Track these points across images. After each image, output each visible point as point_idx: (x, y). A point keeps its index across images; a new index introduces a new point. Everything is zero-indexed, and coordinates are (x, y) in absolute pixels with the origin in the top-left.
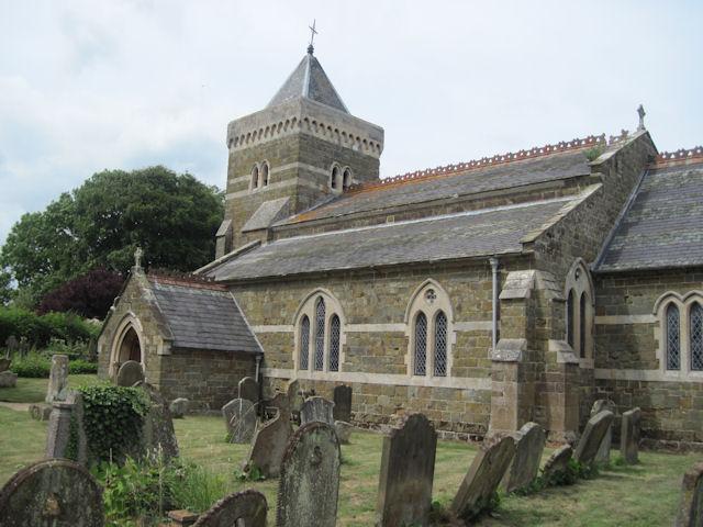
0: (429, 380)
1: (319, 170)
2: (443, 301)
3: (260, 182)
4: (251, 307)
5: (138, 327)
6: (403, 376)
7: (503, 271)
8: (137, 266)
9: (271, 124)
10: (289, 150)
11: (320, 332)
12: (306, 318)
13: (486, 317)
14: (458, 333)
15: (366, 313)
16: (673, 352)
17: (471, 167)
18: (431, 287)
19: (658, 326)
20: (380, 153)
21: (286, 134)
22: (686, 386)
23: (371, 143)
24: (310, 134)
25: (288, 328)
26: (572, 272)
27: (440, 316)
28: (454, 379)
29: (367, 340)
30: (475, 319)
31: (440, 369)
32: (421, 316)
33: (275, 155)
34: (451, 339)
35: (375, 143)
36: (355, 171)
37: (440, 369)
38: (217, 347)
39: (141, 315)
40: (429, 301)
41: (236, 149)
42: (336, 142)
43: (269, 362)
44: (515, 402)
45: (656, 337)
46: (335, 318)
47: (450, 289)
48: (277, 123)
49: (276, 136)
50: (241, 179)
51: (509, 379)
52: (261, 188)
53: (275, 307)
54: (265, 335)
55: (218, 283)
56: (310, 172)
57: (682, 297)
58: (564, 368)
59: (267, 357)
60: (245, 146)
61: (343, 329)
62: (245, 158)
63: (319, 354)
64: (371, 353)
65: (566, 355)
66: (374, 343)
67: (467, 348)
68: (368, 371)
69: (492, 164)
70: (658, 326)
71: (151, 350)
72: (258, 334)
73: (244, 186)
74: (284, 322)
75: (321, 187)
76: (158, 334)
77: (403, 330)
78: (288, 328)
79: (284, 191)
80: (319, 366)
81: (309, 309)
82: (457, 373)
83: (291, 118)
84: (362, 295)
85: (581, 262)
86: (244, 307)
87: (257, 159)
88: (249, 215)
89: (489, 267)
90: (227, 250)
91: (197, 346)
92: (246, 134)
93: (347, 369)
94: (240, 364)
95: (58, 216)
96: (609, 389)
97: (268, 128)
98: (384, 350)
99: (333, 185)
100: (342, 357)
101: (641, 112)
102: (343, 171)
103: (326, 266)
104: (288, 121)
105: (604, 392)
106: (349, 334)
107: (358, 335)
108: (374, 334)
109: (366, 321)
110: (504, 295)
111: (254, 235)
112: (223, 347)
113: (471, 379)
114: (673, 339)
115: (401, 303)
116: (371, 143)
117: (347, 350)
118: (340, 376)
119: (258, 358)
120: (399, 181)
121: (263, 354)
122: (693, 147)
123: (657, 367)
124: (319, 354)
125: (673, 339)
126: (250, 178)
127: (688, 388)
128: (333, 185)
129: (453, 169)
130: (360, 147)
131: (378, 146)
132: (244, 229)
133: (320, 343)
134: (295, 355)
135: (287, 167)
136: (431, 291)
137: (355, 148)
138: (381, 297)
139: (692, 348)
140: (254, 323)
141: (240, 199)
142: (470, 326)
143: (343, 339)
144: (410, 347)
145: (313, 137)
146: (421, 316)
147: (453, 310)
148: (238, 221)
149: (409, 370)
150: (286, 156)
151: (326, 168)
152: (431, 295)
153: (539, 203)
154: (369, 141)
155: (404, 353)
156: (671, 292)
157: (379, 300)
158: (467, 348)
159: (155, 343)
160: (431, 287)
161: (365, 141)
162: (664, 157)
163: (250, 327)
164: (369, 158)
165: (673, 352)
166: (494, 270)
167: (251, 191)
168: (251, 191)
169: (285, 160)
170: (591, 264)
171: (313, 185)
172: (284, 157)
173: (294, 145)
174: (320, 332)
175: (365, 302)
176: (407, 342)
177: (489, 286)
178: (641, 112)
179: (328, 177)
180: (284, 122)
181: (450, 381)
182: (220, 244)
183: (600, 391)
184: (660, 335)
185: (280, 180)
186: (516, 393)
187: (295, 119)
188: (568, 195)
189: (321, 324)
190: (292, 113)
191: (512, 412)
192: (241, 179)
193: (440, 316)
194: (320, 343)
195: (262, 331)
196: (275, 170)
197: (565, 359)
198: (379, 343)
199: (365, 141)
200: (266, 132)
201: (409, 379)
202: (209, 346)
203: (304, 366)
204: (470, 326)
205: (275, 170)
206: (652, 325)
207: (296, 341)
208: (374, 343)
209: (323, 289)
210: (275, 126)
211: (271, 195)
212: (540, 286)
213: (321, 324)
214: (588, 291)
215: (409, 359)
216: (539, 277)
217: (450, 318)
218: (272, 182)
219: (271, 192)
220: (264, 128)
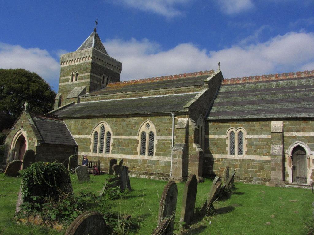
0: (146, 157)
1: (98, 77)
2: (153, 128)
3: (74, 79)
4: (73, 127)
5: (25, 134)
6: (136, 155)
7: (176, 118)
8: (25, 109)
9: (80, 57)
10: (87, 68)
11: (102, 138)
12: (96, 133)
13: (169, 134)
14: (158, 140)
15: (122, 131)
16: (232, 148)
17: (128, 83)
18: (148, 122)
19: (227, 139)
20: (120, 72)
21: (86, 62)
22: (236, 160)
23: (117, 68)
24: (95, 62)
25: (89, 136)
26: (199, 119)
27: (151, 134)
28: (157, 157)
29: (122, 142)
30: (165, 135)
31: (151, 153)
32: (143, 134)
33: (81, 69)
34: (156, 142)
35: (119, 68)
36: (111, 78)
37: (151, 153)
38: (60, 143)
39: (27, 130)
40: (147, 128)
41: (64, 66)
42: (105, 66)
43: (79, 150)
44: (181, 166)
45: (226, 143)
46: (109, 134)
47: (156, 124)
48: (82, 57)
49: (81, 62)
50: (66, 78)
51: (179, 157)
52: (74, 81)
53: (83, 128)
54: (78, 139)
55: (59, 118)
56: (95, 77)
57: (236, 129)
58: (198, 154)
59: (79, 147)
60: (68, 65)
61: (112, 137)
62: (68, 69)
63: (102, 147)
64: (122, 146)
65: (199, 149)
66: (125, 143)
67: (161, 145)
68: (122, 153)
69: (123, 84)
70: (227, 139)
71: (31, 144)
72: (76, 138)
73: (67, 80)
74: (87, 134)
75: (99, 83)
76: (35, 138)
77: (137, 138)
78: (89, 136)
79: (84, 83)
80: (101, 151)
81: (98, 129)
82: (157, 154)
83: (88, 56)
84: (120, 124)
85: (202, 116)
86: (70, 127)
87: (73, 70)
88: (69, 92)
89: (171, 116)
90: (59, 106)
91: (51, 143)
92: (69, 60)
93: (113, 152)
94: (68, 150)
95: (37, 74)
96: (209, 161)
97: (78, 59)
98: (129, 145)
99: (103, 82)
100: (111, 148)
101: (219, 64)
102: (107, 78)
103: (139, 112)
104: (75, 59)
105: (207, 162)
106: (114, 139)
107: (118, 139)
108: (124, 139)
109: (122, 134)
110: (177, 126)
111: (72, 100)
112: (62, 143)
113: (163, 157)
114: (233, 143)
115: (136, 128)
116: (117, 68)
117: (113, 145)
118: (111, 155)
119: (76, 148)
120: (125, 82)
121: (77, 146)
122: (230, 78)
123: (226, 153)
124: (102, 147)
125: (233, 143)
126: (70, 77)
127: (237, 161)
128: (103, 82)
129: (126, 83)
130: (113, 69)
131: (120, 69)
132: (68, 97)
133: (102, 143)
134: (92, 147)
135: (86, 74)
136: (148, 124)
137: (112, 69)
138: (128, 125)
139: (239, 147)
140: (74, 134)
141: (66, 85)
142: (163, 137)
143: (112, 141)
144: (139, 145)
145: (96, 64)
146: (143, 134)
147: (157, 131)
148: (64, 94)
149: (139, 153)
150: (85, 70)
151: (101, 76)
152: (148, 125)
153: (185, 94)
154: (117, 67)
155: (137, 146)
156: (103, 122)
157: (127, 127)
158: (161, 145)
159: (33, 141)
160: (148, 122)
161: (115, 67)
162: (226, 80)
163: (72, 136)
164: (117, 73)
165: (232, 148)
166: (173, 117)
167: (70, 83)
168: (70, 83)
169: (85, 72)
170: (204, 116)
171: (96, 82)
172: (84, 70)
173: (89, 66)
174: (102, 138)
175: (121, 127)
176: (138, 143)
177: (171, 123)
178: (219, 64)
179: (101, 79)
180: (85, 57)
181: (155, 158)
182: (57, 102)
183: (206, 162)
184: (228, 142)
185: (82, 79)
186: (182, 163)
187: (90, 56)
188: (197, 91)
189: (102, 135)
190: (88, 54)
191: (180, 170)
192: (66, 78)
193: (151, 134)
194: (102, 143)
195: (77, 137)
196: (81, 75)
197: (199, 150)
198: (127, 143)
199: (115, 67)
200: (77, 60)
201: (139, 157)
202: (56, 143)
203: (95, 151)
204: (163, 137)
205: (81, 75)
206: (225, 139)
207: (92, 141)
208: (125, 143)
209: (104, 122)
210: (81, 58)
211: (79, 85)
212: (190, 124)
213: (102, 135)
214: (203, 126)
215: (139, 149)
216: (190, 120)
217: (155, 134)
218: (79, 79)
219: (78, 83)
220: (77, 58)
